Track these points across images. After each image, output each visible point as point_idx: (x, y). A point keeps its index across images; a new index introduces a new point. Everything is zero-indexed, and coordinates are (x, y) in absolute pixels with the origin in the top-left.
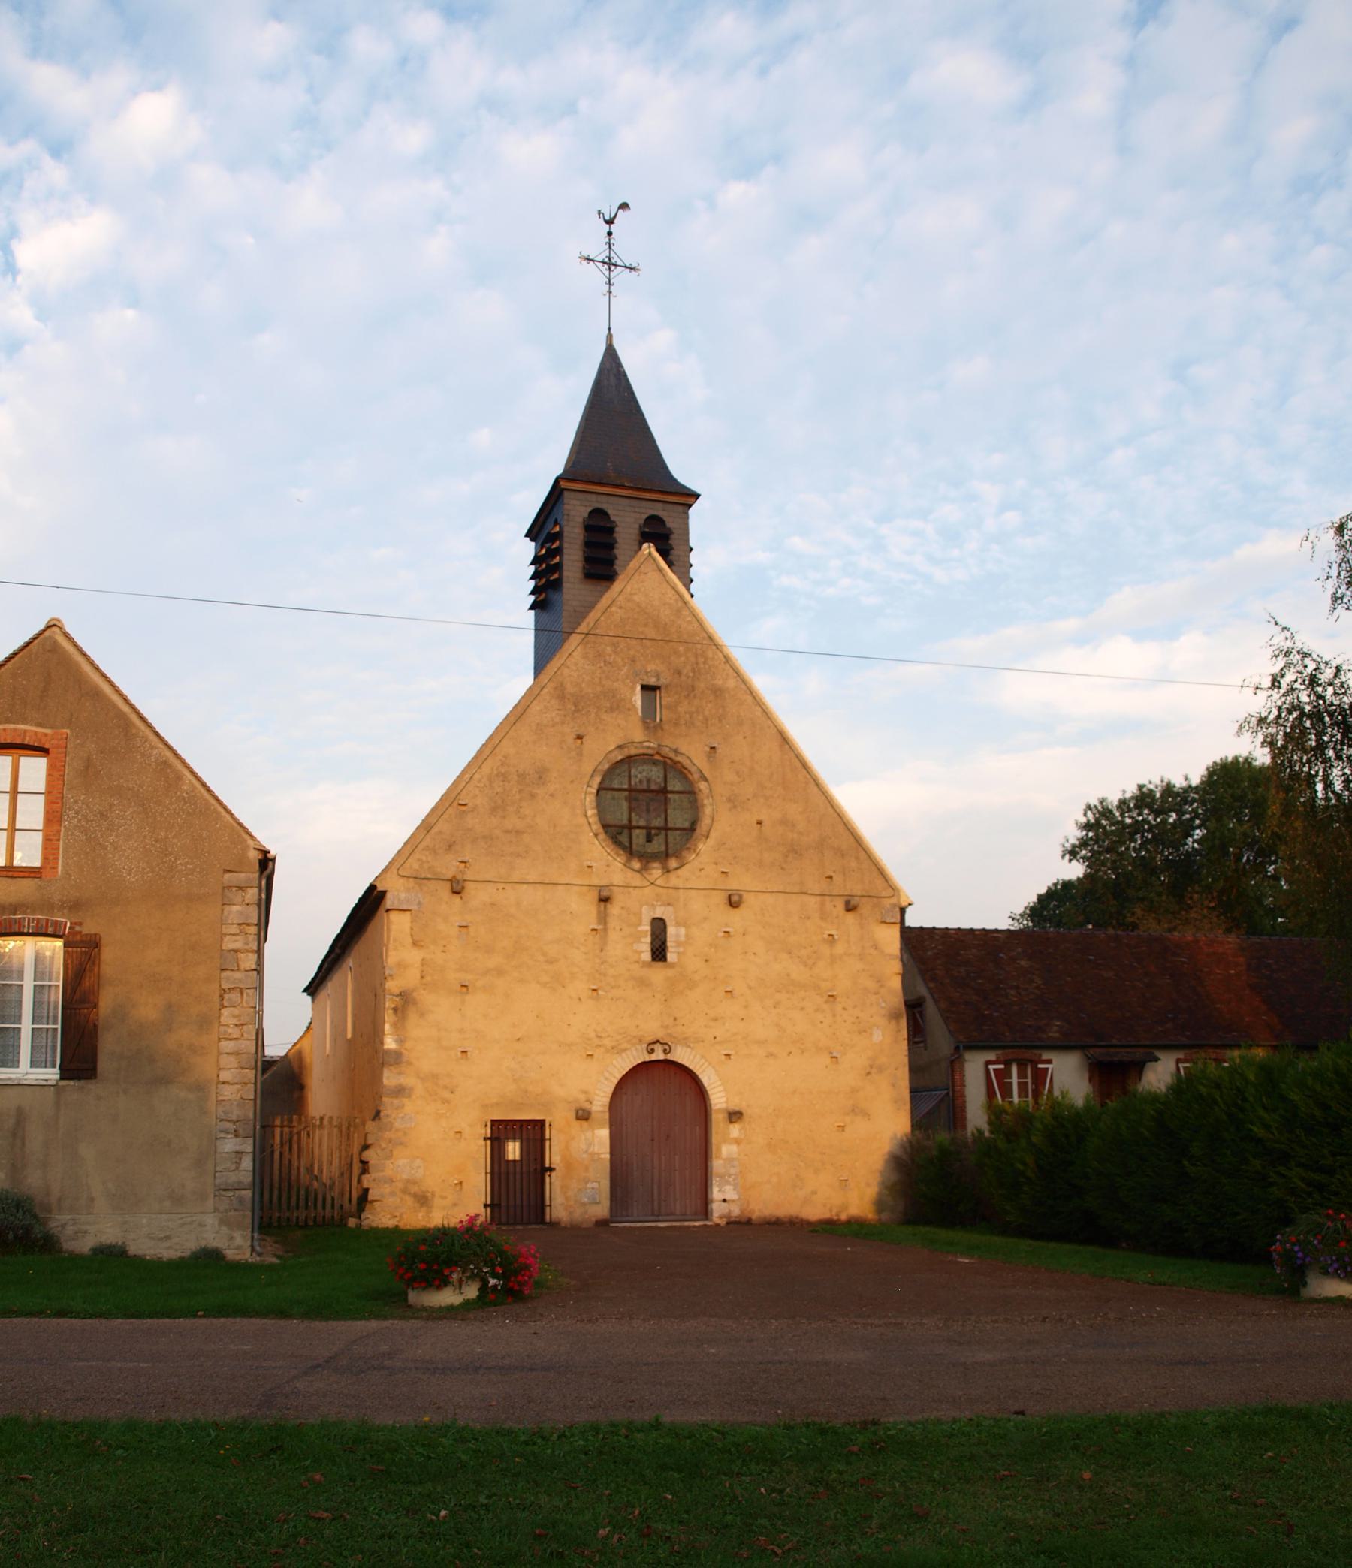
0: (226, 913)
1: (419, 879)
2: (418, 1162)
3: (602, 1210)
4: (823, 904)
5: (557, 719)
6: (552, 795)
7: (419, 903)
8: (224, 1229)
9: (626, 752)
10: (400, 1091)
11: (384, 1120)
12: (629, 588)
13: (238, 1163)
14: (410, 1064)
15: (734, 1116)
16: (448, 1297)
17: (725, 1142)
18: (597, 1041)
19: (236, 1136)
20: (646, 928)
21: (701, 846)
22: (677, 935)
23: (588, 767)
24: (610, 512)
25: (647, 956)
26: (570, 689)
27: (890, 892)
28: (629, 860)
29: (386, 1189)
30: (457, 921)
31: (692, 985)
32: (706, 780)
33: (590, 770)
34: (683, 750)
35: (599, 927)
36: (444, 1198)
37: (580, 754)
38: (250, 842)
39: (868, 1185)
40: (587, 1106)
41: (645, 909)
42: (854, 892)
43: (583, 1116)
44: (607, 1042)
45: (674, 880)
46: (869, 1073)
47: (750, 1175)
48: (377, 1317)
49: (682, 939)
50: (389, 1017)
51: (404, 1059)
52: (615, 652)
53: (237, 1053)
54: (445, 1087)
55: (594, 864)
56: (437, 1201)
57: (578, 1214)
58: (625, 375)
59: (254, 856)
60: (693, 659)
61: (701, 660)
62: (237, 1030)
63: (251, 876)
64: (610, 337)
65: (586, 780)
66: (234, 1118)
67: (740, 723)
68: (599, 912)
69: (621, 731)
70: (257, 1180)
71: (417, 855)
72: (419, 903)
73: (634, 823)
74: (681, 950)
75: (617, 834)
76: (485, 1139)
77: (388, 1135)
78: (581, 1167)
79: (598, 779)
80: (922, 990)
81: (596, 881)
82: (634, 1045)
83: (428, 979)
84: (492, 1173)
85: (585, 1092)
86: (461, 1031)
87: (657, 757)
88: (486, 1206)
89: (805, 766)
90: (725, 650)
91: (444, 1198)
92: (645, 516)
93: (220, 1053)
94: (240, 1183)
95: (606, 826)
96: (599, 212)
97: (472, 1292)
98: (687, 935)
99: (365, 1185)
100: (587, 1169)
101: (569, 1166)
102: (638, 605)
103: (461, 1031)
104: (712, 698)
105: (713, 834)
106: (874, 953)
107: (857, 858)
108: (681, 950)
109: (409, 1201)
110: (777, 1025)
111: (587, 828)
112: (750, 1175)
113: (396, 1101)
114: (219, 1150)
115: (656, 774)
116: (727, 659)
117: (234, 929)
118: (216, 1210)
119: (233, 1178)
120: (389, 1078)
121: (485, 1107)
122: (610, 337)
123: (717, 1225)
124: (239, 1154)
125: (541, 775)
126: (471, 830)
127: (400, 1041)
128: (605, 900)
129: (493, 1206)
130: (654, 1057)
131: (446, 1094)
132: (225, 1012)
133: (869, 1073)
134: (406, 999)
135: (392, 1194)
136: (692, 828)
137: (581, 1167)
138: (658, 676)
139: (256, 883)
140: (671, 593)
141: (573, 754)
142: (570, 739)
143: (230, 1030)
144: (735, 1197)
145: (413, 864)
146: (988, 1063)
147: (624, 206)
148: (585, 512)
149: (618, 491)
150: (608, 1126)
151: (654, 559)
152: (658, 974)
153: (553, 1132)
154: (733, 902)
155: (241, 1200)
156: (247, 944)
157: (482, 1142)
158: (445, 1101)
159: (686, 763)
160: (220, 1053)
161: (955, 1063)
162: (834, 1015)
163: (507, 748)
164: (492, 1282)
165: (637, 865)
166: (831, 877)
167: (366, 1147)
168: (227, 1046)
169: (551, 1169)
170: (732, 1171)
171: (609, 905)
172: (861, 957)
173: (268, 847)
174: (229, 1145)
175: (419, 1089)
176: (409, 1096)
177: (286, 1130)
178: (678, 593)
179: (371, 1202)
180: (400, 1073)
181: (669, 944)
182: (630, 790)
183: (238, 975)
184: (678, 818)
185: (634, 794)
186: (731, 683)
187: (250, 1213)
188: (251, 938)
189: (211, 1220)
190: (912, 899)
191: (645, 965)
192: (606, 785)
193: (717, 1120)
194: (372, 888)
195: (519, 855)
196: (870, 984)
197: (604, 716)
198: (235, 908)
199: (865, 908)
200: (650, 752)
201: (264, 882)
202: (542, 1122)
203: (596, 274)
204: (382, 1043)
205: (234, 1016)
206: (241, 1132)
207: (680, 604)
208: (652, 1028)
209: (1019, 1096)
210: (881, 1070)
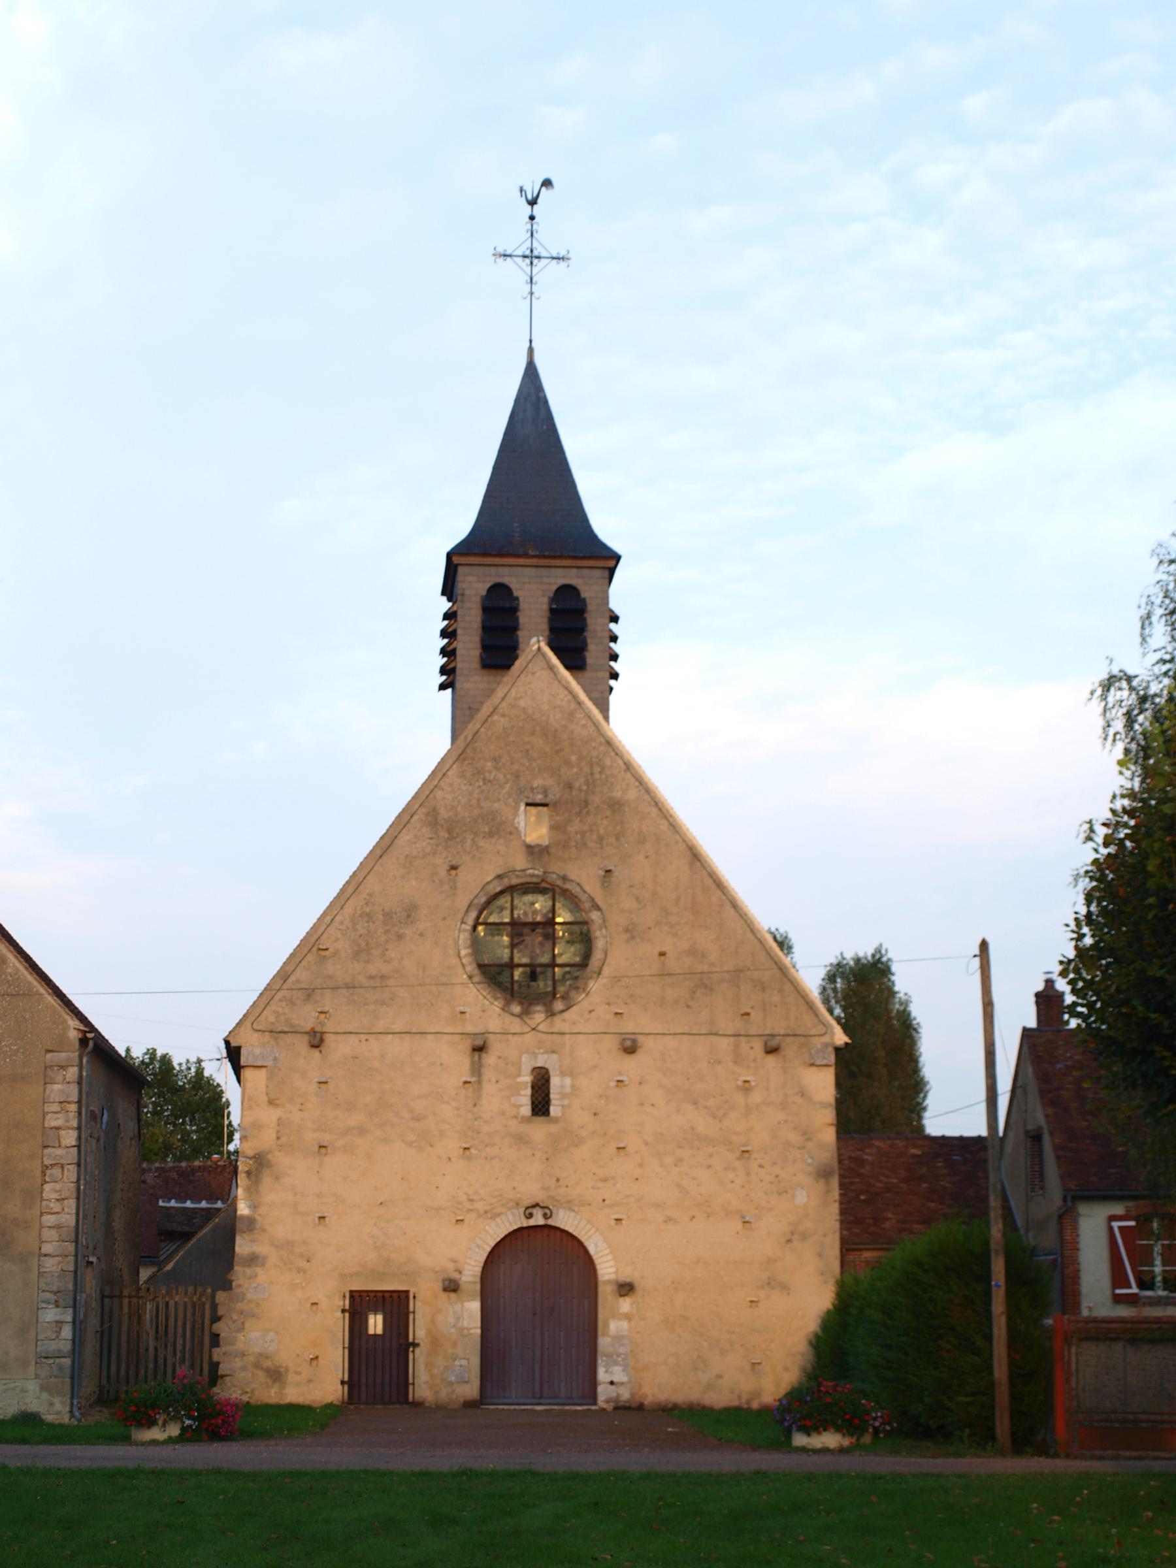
0: (48, 1092)
1: (275, 1033)
2: (271, 1335)
3: (471, 1390)
4: (737, 1046)
5: (428, 850)
6: (421, 935)
7: (275, 1059)
8: (45, 1395)
9: (506, 882)
10: (253, 1260)
11: (236, 1291)
12: (513, 691)
13: (58, 1332)
14: (264, 1231)
15: (626, 1289)
16: (155, 1434)
17: (614, 1316)
18: (467, 1205)
19: (57, 1306)
20: (527, 1079)
21: (591, 983)
22: (562, 1087)
23: (462, 902)
24: (513, 586)
25: (526, 1110)
26: (444, 814)
27: (821, 1029)
28: (508, 1003)
29: (238, 1363)
30: (316, 1076)
31: (578, 1142)
32: (598, 908)
33: (465, 903)
34: (572, 876)
35: (473, 1079)
36: (298, 1373)
37: (454, 888)
39: (786, 1369)
40: (455, 1276)
41: (525, 1058)
42: (776, 1031)
43: (452, 1287)
44: (479, 1206)
45: (559, 1024)
46: (789, 1241)
47: (641, 1354)
49: (568, 1090)
50: (242, 1179)
51: (258, 1226)
52: (496, 768)
53: (58, 1227)
54: (301, 1256)
55: (468, 1010)
56: (291, 1377)
57: (444, 1394)
58: (546, 402)
60: (586, 769)
61: (597, 770)
62: (58, 1203)
63: (72, 1055)
64: (531, 351)
65: (460, 916)
67: (642, 840)
68: (472, 1063)
70: (91, 1346)
71: (273, 1007)
72: (275, 1059)
73: (516, 960)
74: (566, 1102)
75: (494, 975)
76: (343, 1311)
77: (240, 1306)
78: (449, 1341)
81: (470, 1029)
82: (509, 1209)
83: (284, 1139)
84: (351, 1349)
85: (454, 1261)
86: (319, 1195)
87: (544, 885)
88: (343, 1383)
89: (719, 885)
90: (626, 756)
91: (298, 1373)
92: (554, 588)
93: (42, 1227)
94: (59, 1351)
95: (480, 966)
96: (521, 190)
97: (174, 1430)
98: (573, 1086)
99: (215, 1359)
100: (455, 1345)
102: (524, 710)
103: (319, 1195)
104: (608, 813)
105: (606, 971)
106: (798, 1100)
107: (781, 991)
108: (566, 1102)
109: (261, 1375)
110: (678, 1186)
111: (460, 969)
112: (641, 1354)
113: (248, 1271)
114: (40, 1320)
116: (629, 766)
117: (55, 1107)
119: (53, 1346)
120: (242, 1246)
121: (343, 1276)
122: (531, 351)
123: (603, 1410)
124: (60, 1323)
125: (410, 913)
126: (331, 977)
127: (254, 1207)
128: (479, 1049)
129: (352, 1383)
130: (532, 1222)
131: (302, 1263)
132: (47, 1187)
133: (789, 1241)
134: (260, 1161)
135: (244, 1368)
136: (584, 964)
137: (449, 1341)
138: (545, 792)
139: (77, 1061)
140: (563, 694)
141: (446, 887)
142: (443, 871)
143: (52, 1205)
144: (625, 1379)
145: (269, 1016)
146: (1113, 1218)
147: (547, 183)
148: (482, 588)
149: (521, 561)
151: (544, 655)
152: (540, 1130)
153: (418, 1304)
154: (630, 1048)
155: (61, 1368)
156: (67, 1121)
157: (339, 1314)
158: (300, 1270)
160: (42, 1227)
161: (1066, 1217)
162: (748, 1174)
163: (372, 884)
164: (188, 1422)
165: (516, 1009)
166: (748, 1014)
167: (216, 1318)
168: (49, 1220)
169: (415, 1345)
170: (622, 1350)
171: (484, 1055)
172: (783, 1106)
174: (50, 1315)
175: (273, 1258)
176: (263, 1265)
177: (134, 1300)
178: (571, 692)
179: (223, 1376)
180: (253, 1241)
181: (552, 1096)
183: (59, 1152)
185: (518, 929)
186: (632, 794)
187: (68, 1380)
188: (72, 1115)
189: (32, 1386)
191: (525, 1120)
193: (606, 1292)
195: (383, 1003)
196: (794, 1137)
197: (482, 843)
198: (57, 1087)
199: (790, 1049)
200: (534, 880)
202: (407, 1292)
203: (516, 271)
204: (236, 1210)
205: (56, 1191)
207: (573, 705)
208: (532, 1191)
209: (1164, 1264)
210: (804, 1237)
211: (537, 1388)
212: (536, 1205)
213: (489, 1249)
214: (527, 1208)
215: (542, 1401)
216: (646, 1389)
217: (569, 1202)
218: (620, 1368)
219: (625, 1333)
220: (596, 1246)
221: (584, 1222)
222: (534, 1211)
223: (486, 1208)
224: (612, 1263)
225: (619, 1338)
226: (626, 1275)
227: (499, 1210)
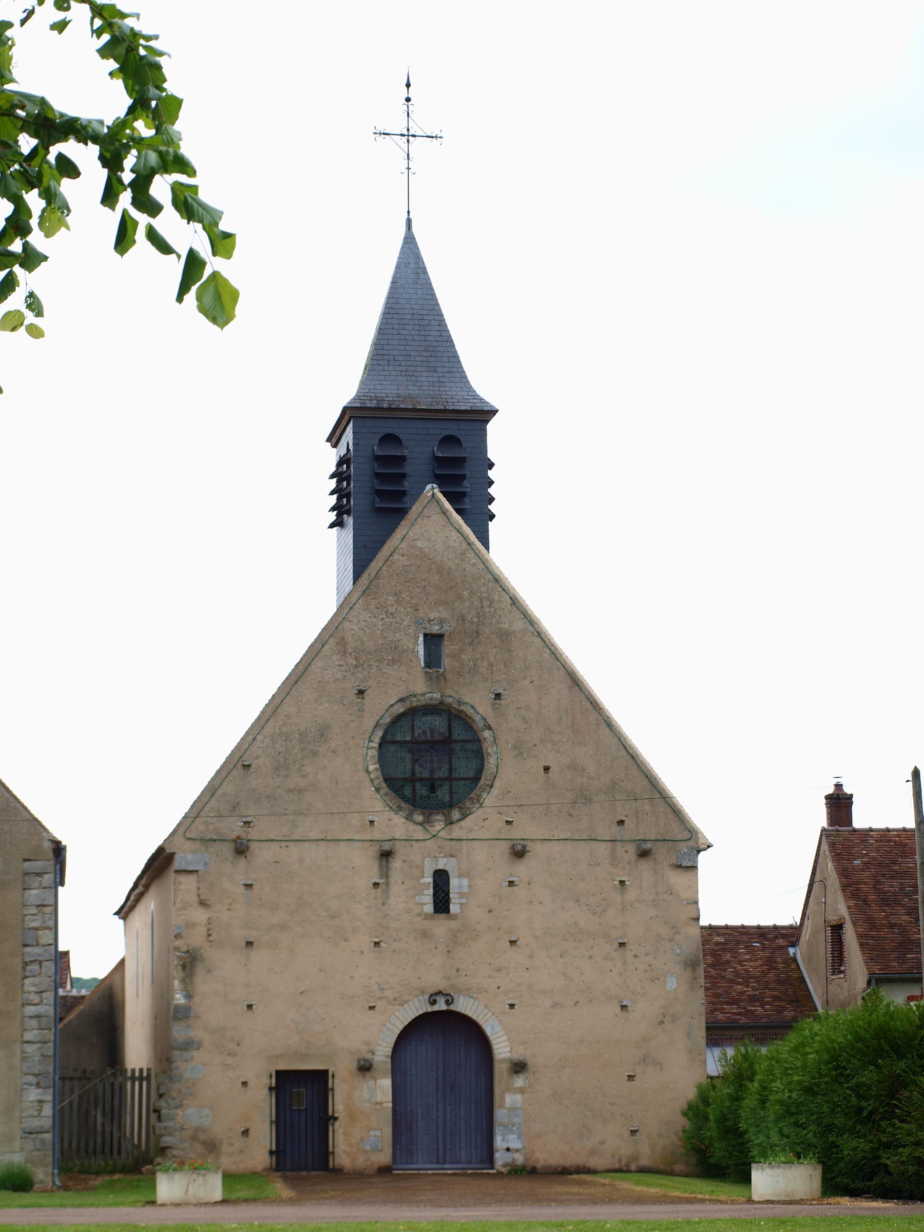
0: (26, 897)
2: (206, 1111)
4: (613, 850)
5: (339, 676)
7: (205, 864)
9: (408, 704)
13: (40, 1111)
15: (519, 1067)
22: (460, 887)
23: (369, 723)
25: (429, 908)
26: (351, 644)
32: (490, 728)
38: (44, 834)
43: (365, 1068)
46: (662, 1022)
53: (38, 1016)
55: (375, 819)
59: (47, 845)
60: (477, 603)
61: (486, 603)
63: (47, 863)
66: (36, 1071)
68: (381, 866)
69: (408, 682)
72: (205, 864)
74: (464, 901)
77: (177, 1086)
79: (380, 733)
80: (841, 908)
81: (378, 836)
82: (416, 996)
85: (368, 1044)
88: (271, 1153)
98: (470, 886)
101: (353, 1116)
104: (498, 642)
105: (497, 783)
110: (564, 974)
115: (439, 723)
118: (22, 1149)
119: (35, 1123)
125: (323, 731)
127: (189, 996)
128: (386, 855)
130: (436, 1008)
133: (662, 1022)
136: (477, 778)
139: (52, 869)
140: (455, 534)
150: (390, 1075)
151: (438, 501)
152: (441, 926)
153: (336, 1081)
155: (43, 1141)
159: (470, 711)
162: (625, 963)
168: (31, 1010)
169: (336, 1119)
170: (516, 1120)
173: (59, 838)
174: (33, 1094)
181: (451, 895)
182: (414, 742)
183: (38, 950)
184: (463, 768)
186: (519, 625)
187: (50, 1153)
190: (711, 840)
191: (427, 917)
192: (389, 738)
193: (500, 1069)
194: (160, 850)
197: (387, 669)
198: (34, 892)
199: (661, 852)
201: (58, 866)
202: (325, 1072)
204: (173, 998)
206: (42, 1083)
207: (465, 546)
208: (435, 980)
212: (439, 993)
213: (398, 1032)
214: (431, 996)
215: (446, 1166)
217: (467, 989)
218: (515, 1136)
219: (519, 1105)
220: (493, 1028)
221: (481, 1007)
222: (438, 998)
224: (507, 1043)
225: (513, 1109)
226: (519, 1054)
227: (405, 998)
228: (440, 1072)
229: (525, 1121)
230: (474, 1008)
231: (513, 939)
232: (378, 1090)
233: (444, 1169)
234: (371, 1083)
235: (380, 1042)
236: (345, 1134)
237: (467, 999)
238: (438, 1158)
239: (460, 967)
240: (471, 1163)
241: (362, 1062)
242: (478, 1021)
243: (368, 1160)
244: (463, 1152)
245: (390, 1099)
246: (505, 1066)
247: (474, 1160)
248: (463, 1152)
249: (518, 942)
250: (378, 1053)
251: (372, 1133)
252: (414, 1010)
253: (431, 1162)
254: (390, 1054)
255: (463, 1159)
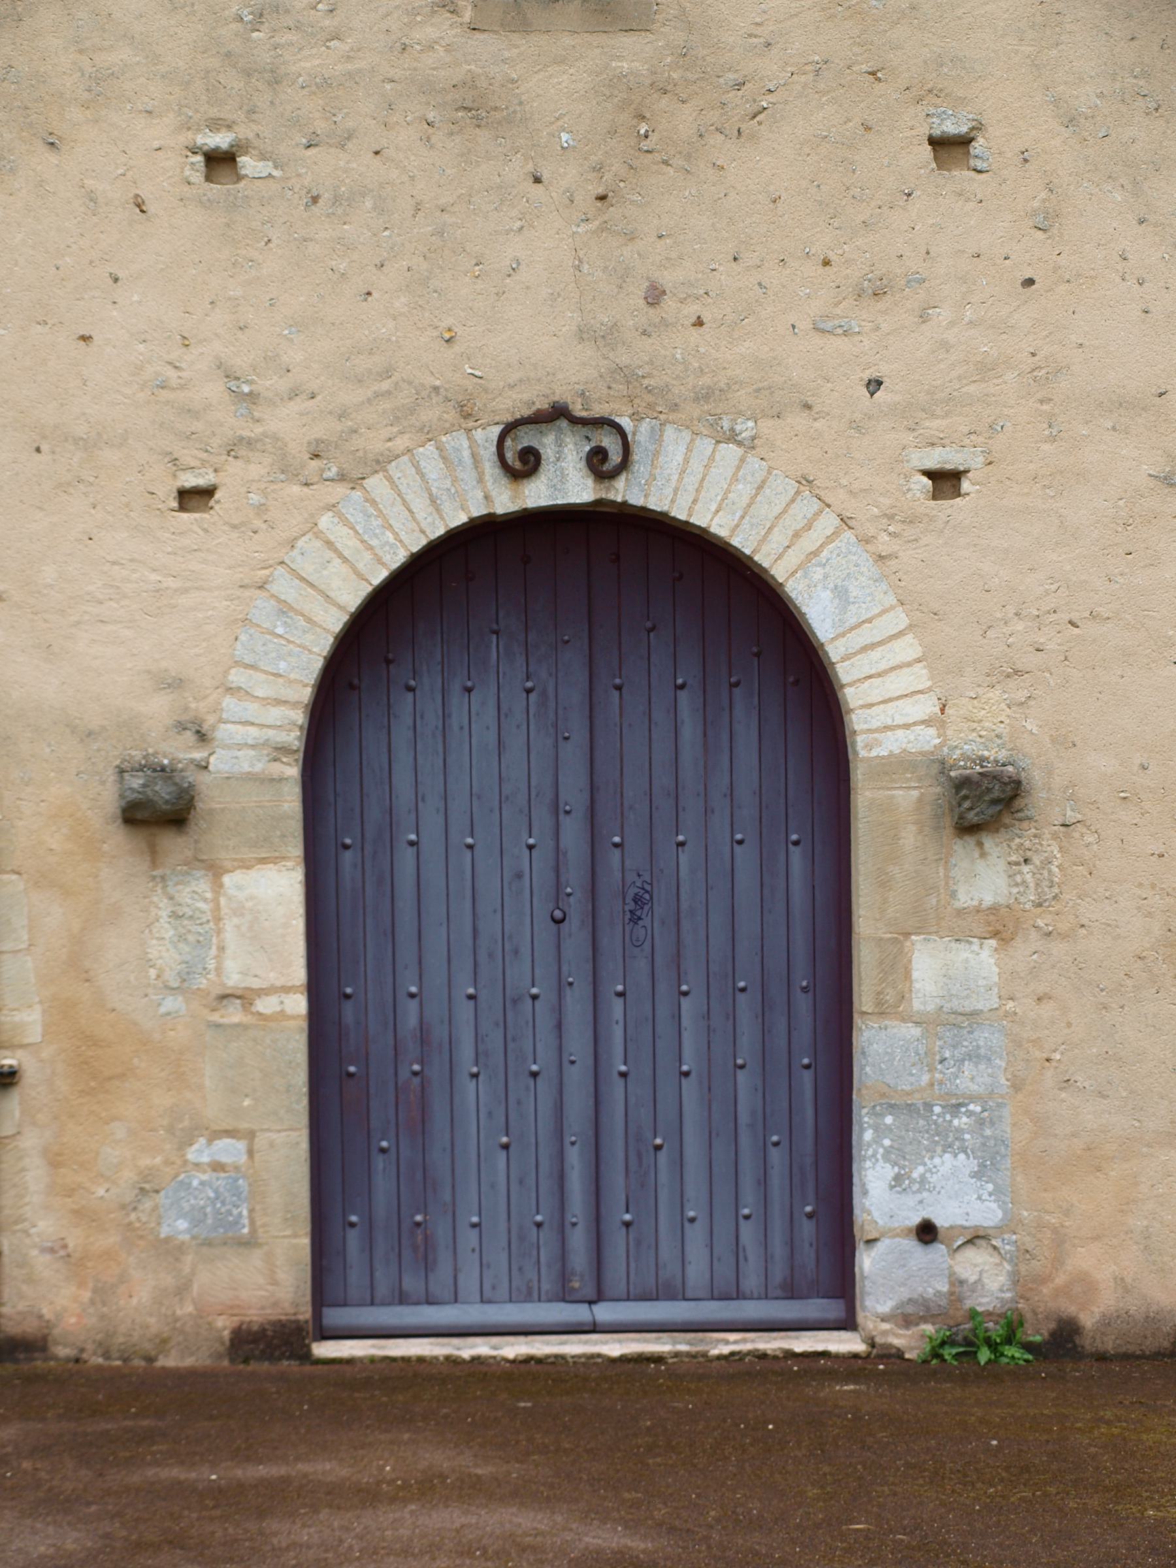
3: (269, 1276)
15: (984, 802)
40: (179, 751)
43: (159, 813)
48: (393, 1360)
51: (123, 803)
82: (429, 434)
85: (176, 684)
130: (537, 494)
150: (296, 849)
193: (888, 814)
208: (536, 351)
211: (580, 1259)
212: (557, 414)
213: (336, 622)
214: (510, 429)
215: (604, 1312)
216: (1084, 1259)
217: (704, 396)
218: (965, 1164)
219: (986, 1002)
220: (841, 594)
221: (782, 487)
222: (547, 443)
223: (322, 429)
224: (919, 677)
225: (955, 1021)
226: (983, 733)
227: (373, 443)
228: (573, 832)
229: (1017, 1085)
230: (743, 491)
231: (951, 128)
232: (229, 925)
233: (594, 1328)
234: (195, 891)
235: (237, 677)
236: (55, 1160)
237: (705, 446)
238: (564, 1277)
239: (667, 278)
240: (738, 1295)
241: (136, 782)
242: (763, 559)
243: (181, 1291)
244: (696, 1236)
245: (299, 973)
246: (907, 796)
247: (752, 1282)
248: (696, 1236)
249: (977, 147)
250: (224, 732)
251: (199, 1152)
252: (420, 505)
253: (528, 1295)
254: (294, 738)
255: (697, 1272)
